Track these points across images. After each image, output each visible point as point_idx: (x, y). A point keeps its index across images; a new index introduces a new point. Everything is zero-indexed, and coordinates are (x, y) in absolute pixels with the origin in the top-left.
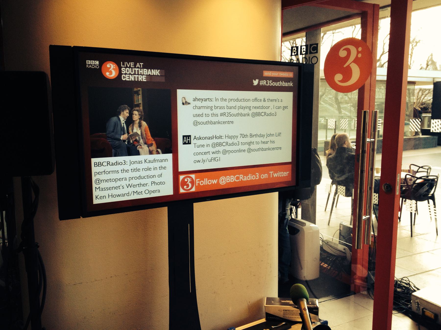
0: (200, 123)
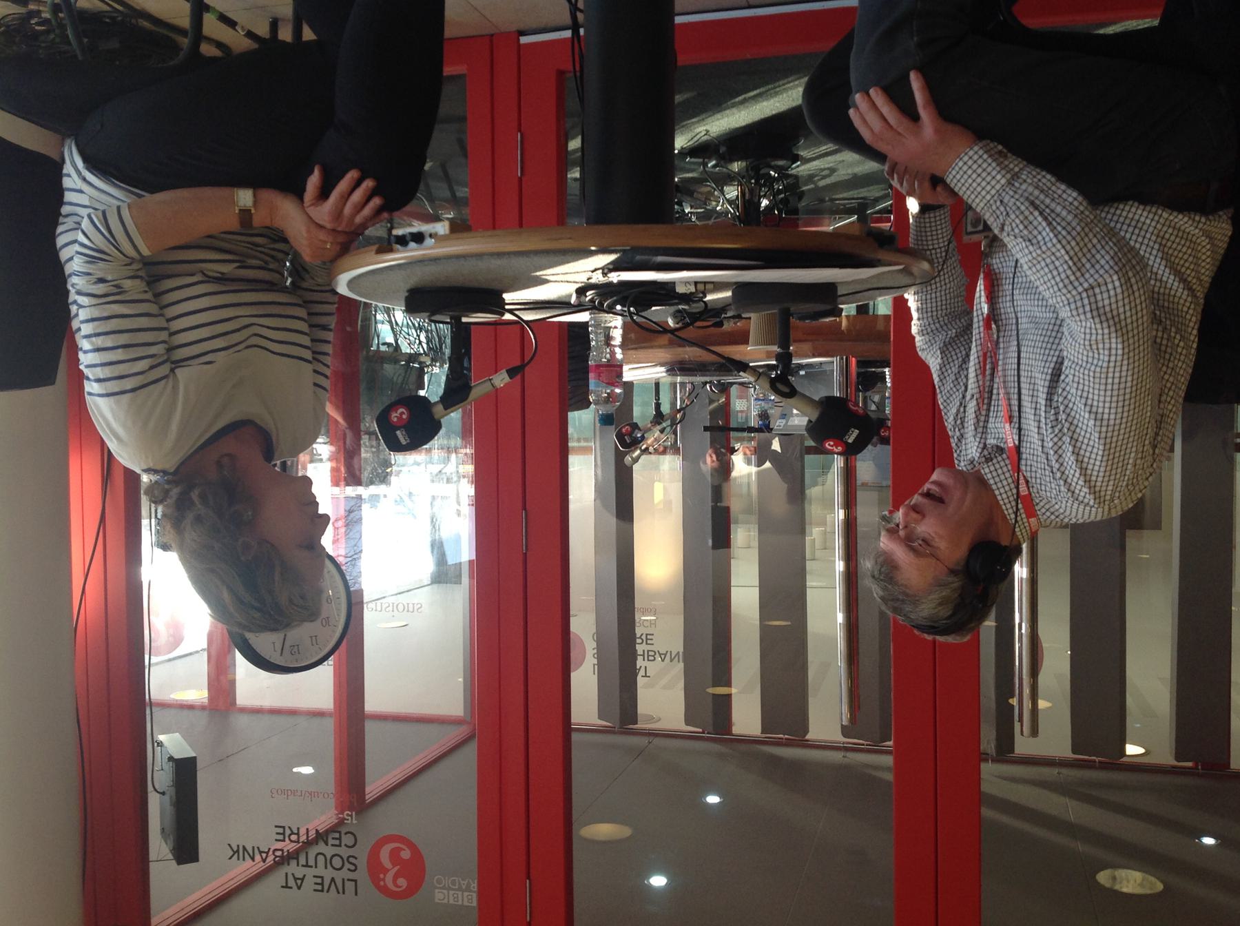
0: (347, 866)
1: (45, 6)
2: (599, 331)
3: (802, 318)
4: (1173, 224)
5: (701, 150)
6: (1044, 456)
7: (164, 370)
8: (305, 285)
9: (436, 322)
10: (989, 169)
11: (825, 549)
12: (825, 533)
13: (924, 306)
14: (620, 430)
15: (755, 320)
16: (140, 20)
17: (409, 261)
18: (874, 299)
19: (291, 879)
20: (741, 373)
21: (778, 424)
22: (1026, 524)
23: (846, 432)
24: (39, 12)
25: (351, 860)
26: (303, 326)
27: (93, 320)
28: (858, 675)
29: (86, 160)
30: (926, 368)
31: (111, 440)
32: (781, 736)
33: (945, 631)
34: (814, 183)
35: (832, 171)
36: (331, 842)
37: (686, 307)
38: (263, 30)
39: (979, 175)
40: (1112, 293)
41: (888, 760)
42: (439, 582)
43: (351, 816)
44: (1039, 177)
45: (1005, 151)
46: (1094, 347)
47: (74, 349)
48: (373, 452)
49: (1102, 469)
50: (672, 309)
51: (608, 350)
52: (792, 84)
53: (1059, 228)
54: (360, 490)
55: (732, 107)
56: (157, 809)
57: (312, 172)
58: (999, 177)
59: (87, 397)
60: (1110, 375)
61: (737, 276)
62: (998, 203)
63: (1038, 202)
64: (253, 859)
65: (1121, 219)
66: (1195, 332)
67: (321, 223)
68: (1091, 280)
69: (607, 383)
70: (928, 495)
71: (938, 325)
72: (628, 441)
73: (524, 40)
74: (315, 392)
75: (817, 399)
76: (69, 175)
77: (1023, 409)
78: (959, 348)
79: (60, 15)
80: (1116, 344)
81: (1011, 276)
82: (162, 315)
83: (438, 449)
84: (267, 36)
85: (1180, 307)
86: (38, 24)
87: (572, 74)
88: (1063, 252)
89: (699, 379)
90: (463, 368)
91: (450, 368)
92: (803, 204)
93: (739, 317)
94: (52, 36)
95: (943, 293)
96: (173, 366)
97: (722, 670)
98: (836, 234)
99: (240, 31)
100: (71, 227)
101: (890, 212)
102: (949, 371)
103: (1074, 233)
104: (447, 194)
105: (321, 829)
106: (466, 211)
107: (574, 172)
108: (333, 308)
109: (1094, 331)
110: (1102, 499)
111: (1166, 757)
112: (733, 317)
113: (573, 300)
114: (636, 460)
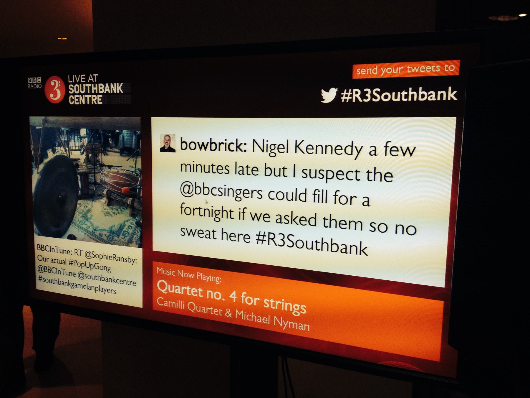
19: (79, 254)
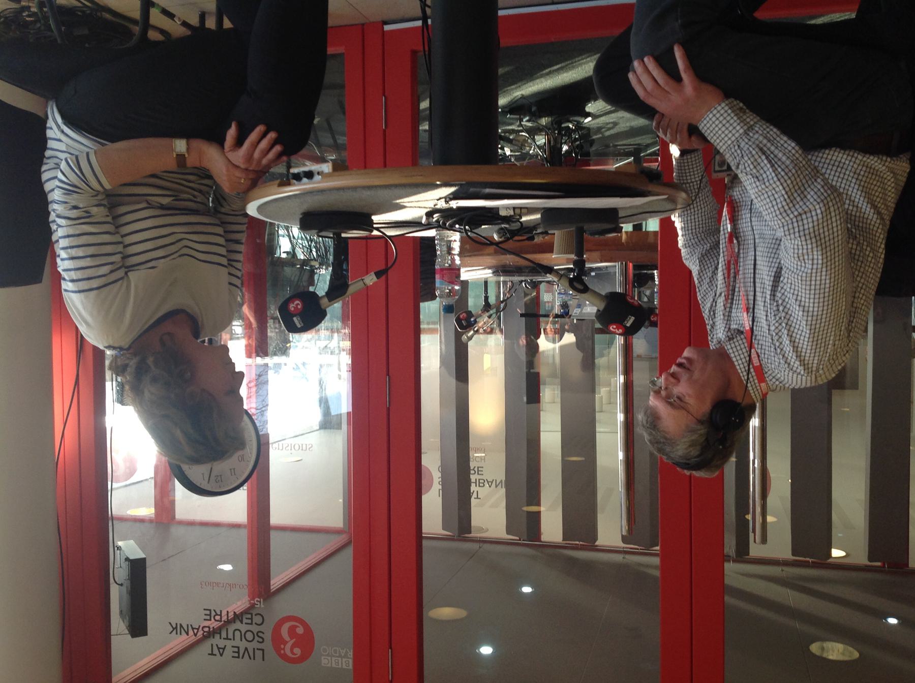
1: (33, 3)
2: (443, 244)
3: (593, 234)
4: (866, 164)
5: (518, 108)
6: (770, 337)
7: (120, 273)
8: (223, 210)
9: (322, 237)
10: (732, 121)
11: (610, 404)
12: (610, 392)
13: (686, 225)
14: (459, 315)
15: (558, 236)
16: (104, 13)
17: (302, 192)
18: (646, 220)
19: (215, 648)
20: (548, 275)
21: (575, 312)
22: (758, 388)
23: (625, 318)
24: (29, 7)
25: (260, 634)
26: (221, 241)
27: (68, 236)
28: (634, 498)
29: (63, 117)
30: (690, 272)
31: (82, 325)
32: (578, 542)
33: (698, 467)
34: (601, 133)
35: (615, 124)
36: (245, 621)
37: (507, 226)
38: (194, 21)
39: (724, 125)
40: (815, 218)
41: (656, 561)
42: (325, 428)
43: (260, 602)
44: (768, 130)
45: (744, 107)
46: (801, 258)
47: (54, 256)
48: (276, 333)
49: (809, 348)
50: (497, 227)
51: (450, 258)
52: (585, 60)
53: (779, 170)
54: (267, 360)
55: (541, 77)
56: (117, 596)
57: (230, 127)
58: (738, 128)
59: (64, 293)
60: (813, 278)
61: (545, 203)
62: (736, 147)
63: (765, 149)
64: (187, 634)
65: (828, 161)
66: (883, 246)
67: (237, 164)
68: (800, 210)
69: (449, 282)
70: (680, 365)
71: (696, 240)
72: (465, 324)
73: (387, 28)
74: (230, 290)
75: (603, 293)
76: (51, 128)
77: (757, 302)
78: (712, 258)
79: (44, 9)
80: (817, 255)
81: (750, 203)
82: (118, 233)
83: (324, 330)
84: (198, 25)
85: (871, 227)
86: (29, 16)
87: (422, 53)
88: (781, 188)
89: (516, 279)
90: (342, 270)
91: (333, 270)
92: (593, 148)
93: (546, 233)
94: (38, 25)
95: (700, 215)
96: (126, 270)
97: (533, 494)
98: (618, 172)
99: (177, 22)
100: (51, 167)
101: (658, 155)
102: (706, 276)
103: (790, 174)
104: (331, 141)
105: (238, 611)
106: (344, 154)
107: (424, 126)
108: (244, 228)
109: (800, 247)
110: (810, 370)
111: (862, 558)
112: (542, 233)
113: (424, 221)
114: (470, 338)
